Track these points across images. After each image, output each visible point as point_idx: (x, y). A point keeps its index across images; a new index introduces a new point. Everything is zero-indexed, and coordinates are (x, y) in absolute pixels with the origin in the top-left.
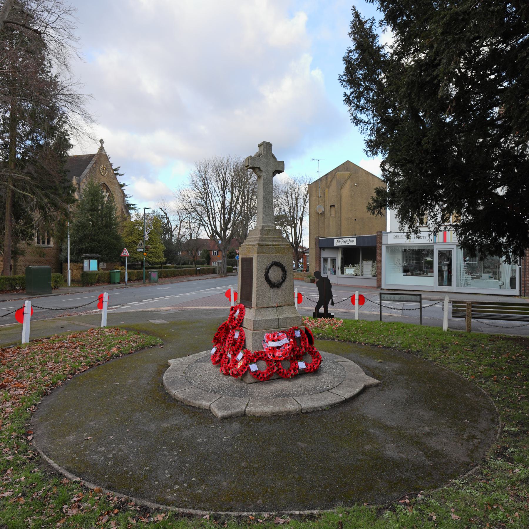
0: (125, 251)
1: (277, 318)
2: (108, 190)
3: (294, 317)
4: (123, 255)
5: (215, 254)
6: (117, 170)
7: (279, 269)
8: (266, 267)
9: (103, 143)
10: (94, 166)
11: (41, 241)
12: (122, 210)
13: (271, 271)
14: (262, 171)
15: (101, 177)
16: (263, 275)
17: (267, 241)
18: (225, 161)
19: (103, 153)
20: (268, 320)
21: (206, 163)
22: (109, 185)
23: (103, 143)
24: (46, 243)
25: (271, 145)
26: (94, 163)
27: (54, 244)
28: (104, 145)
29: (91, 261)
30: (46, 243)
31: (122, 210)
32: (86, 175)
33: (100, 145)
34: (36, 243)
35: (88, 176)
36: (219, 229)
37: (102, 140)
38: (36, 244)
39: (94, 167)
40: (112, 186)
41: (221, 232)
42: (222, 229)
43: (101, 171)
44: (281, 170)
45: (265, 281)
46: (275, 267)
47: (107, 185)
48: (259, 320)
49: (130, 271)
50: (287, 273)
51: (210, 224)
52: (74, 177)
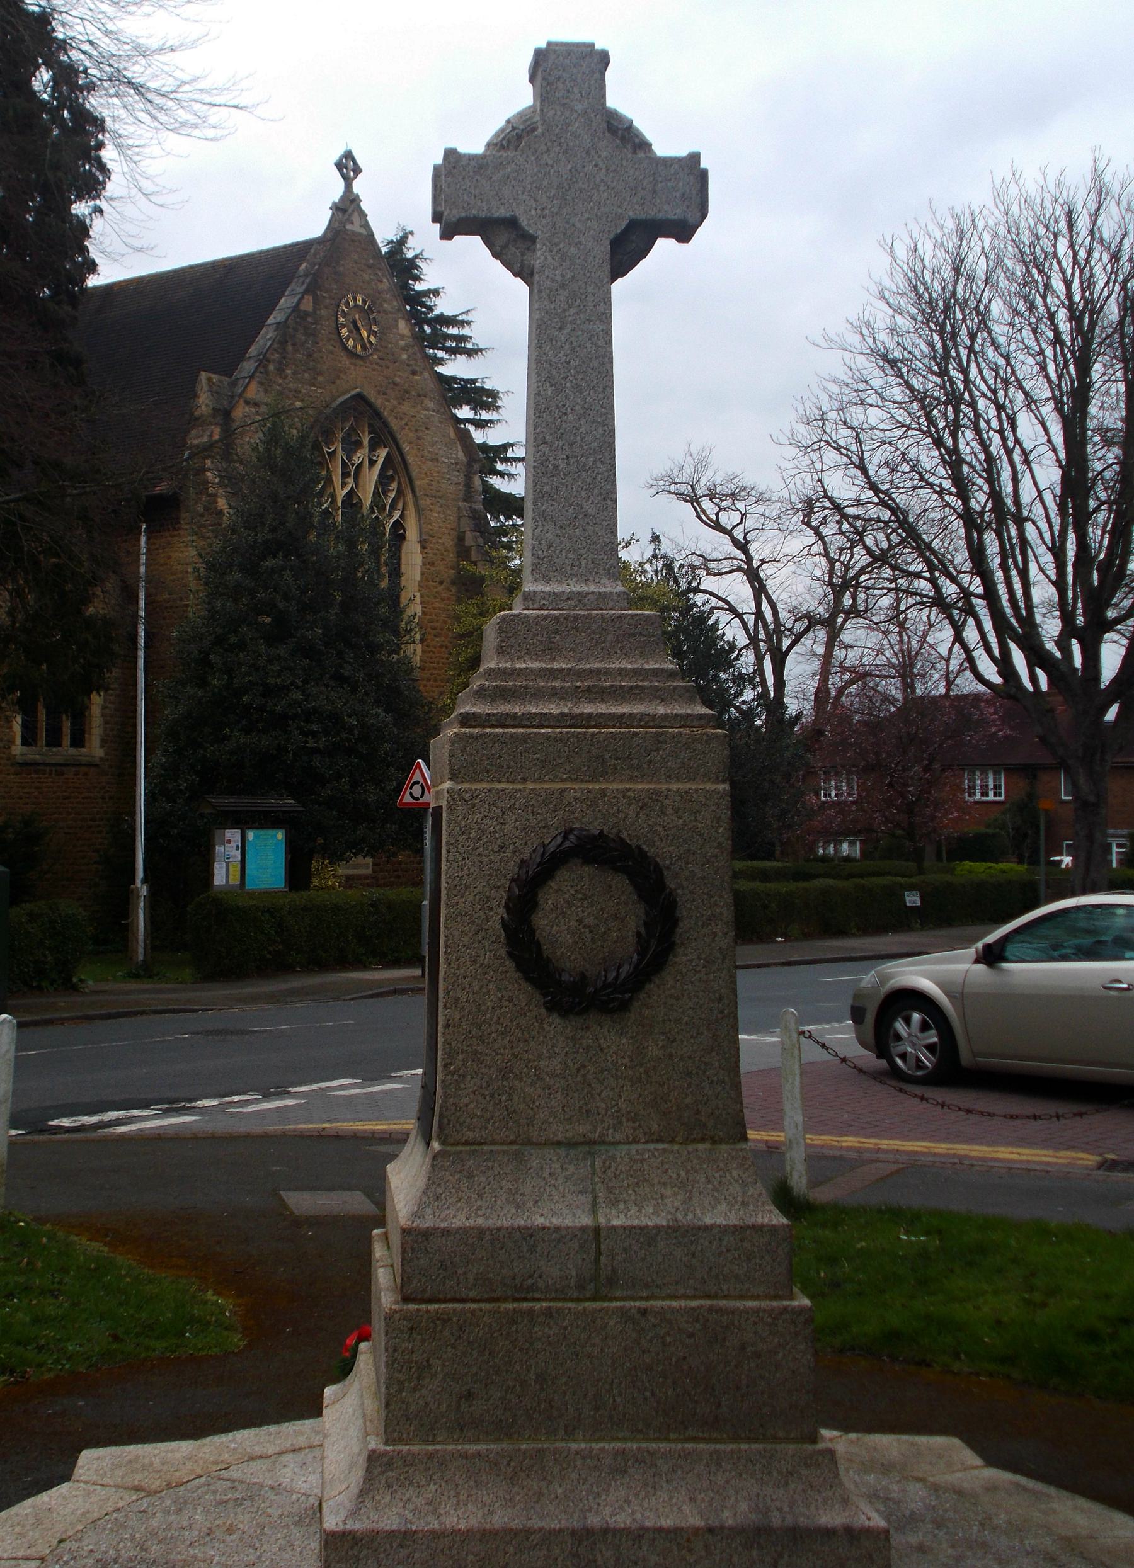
0: (417, 777)
1: (586, 1220)
2: (382, 435)
3: (725, 1230)
4: (408, 799)
5: (985, 794)
6: (463, 323)
7: (620, 883)
8: (512, 870)
9: (357, 170)
10: (308, 305)
11: (42, 735)
12: (461, 539)
13: (550, 898)
14: (533, 239)
15: (346, 361)
16: (495, 924)
17: (537, 695)
18: (1082, 198)
19: (356, 227)
20: (511, 1230)
21: (957, 218)
22: (385, 405)
23: (357, 170)
24: (67, 740)
25: (604, 59)
26: (306, 292)
27: (104, 742)
28: (358, 186)
29: (251, 835)
30: (67, 740)
31: (461, 539)
32: (263, 361)
33: (340, 185)
34: (18, 740)
35: (271, 367)
36: (1050, 627)
37: (349, 155)
38: (18, 749)
39: (307, 314)
40: (406, 407)
41: (1062, 643)
42: (1069, 630)
43: (344, 332)
44: (672, 212)
45: (509, 964)
46: (587, 870)
47: (378, 401)
48: (446, 1232)
49: (404, 893)
50: (681, 912)
51: (990, 595)
52: (204, 375)
